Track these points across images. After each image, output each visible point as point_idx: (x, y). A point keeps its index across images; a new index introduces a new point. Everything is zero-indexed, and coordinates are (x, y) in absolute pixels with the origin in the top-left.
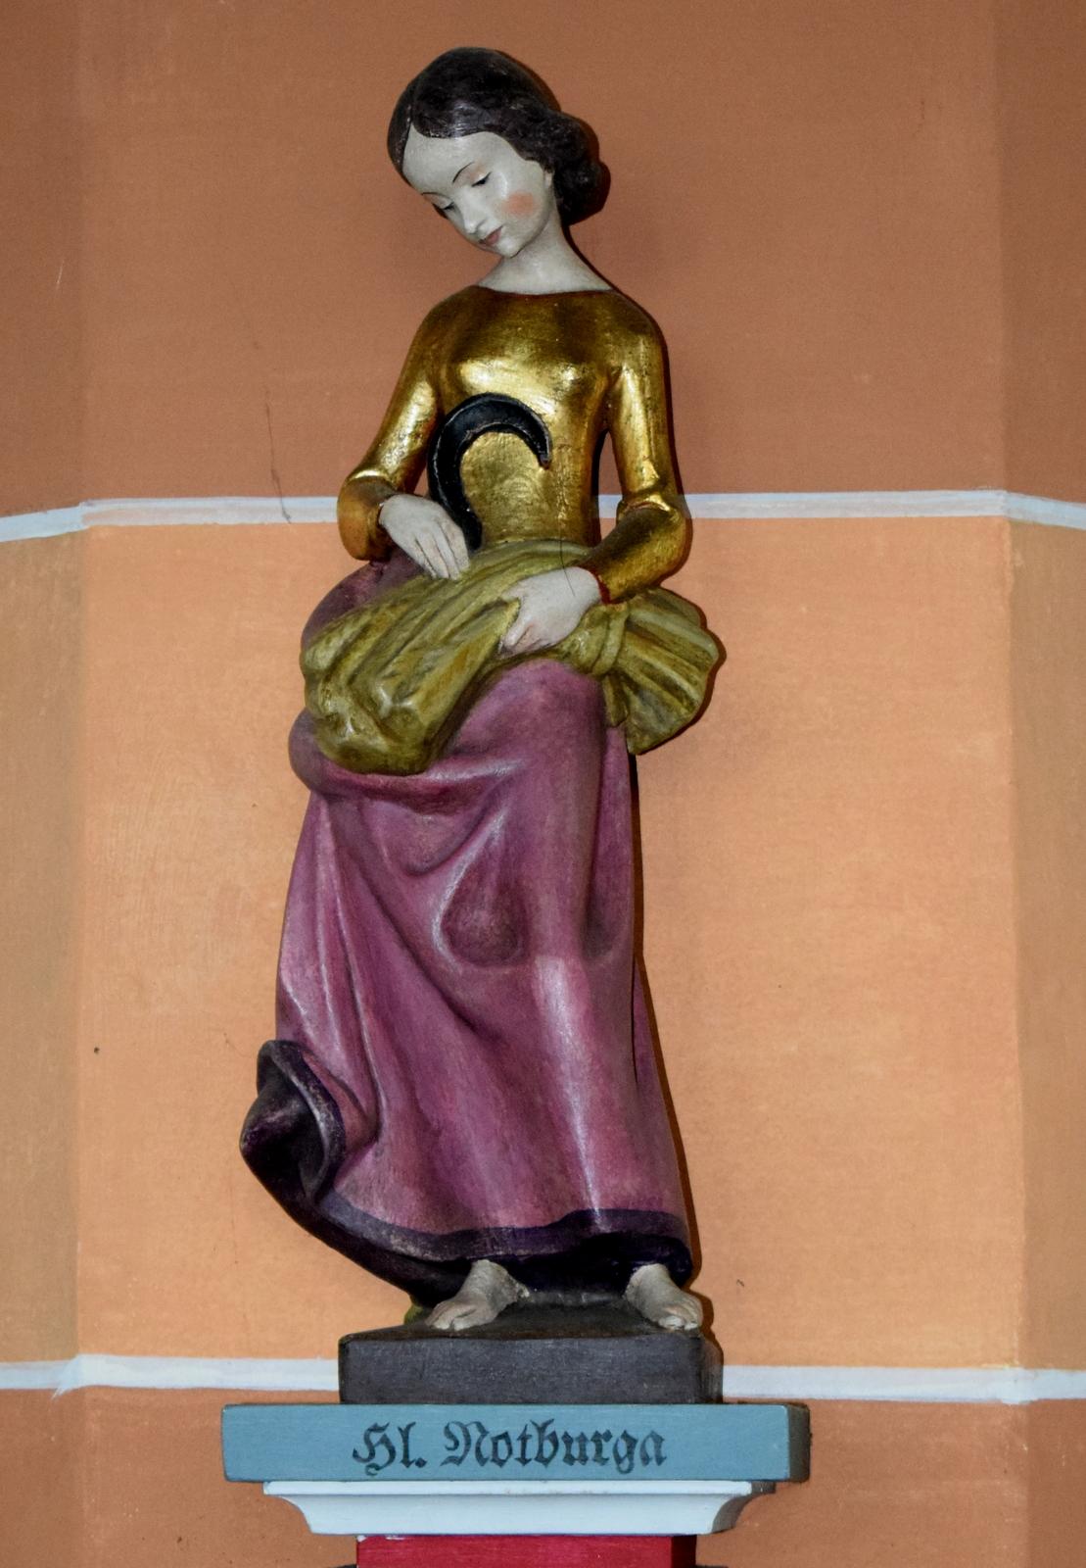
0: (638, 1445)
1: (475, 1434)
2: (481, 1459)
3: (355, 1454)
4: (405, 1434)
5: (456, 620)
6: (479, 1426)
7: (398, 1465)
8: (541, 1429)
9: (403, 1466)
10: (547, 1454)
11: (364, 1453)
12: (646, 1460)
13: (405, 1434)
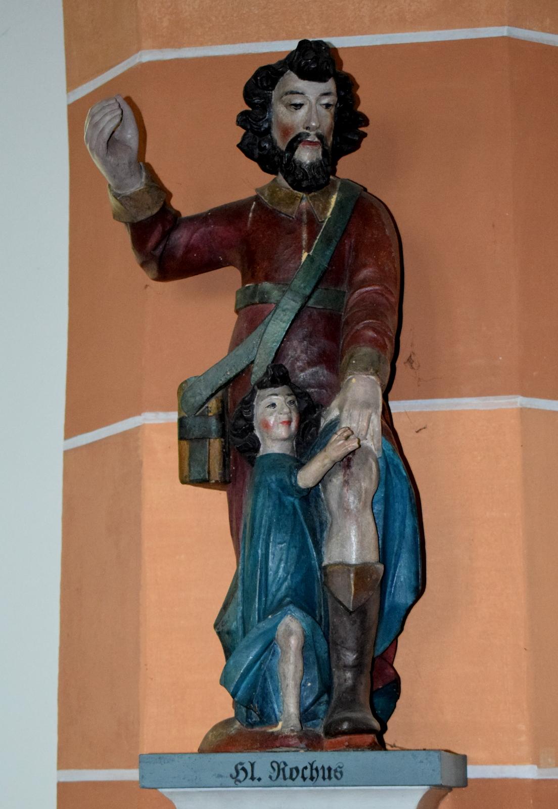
0: (250, 775)
1: (282, 766)
2: (304, 779)
3: (231, 776)
4: (252, 765)
7: (248, 781)
8: (312, 765)
10: (294, 776)
11: (235, 774)
12: (324, 778)
13: (252, 765)
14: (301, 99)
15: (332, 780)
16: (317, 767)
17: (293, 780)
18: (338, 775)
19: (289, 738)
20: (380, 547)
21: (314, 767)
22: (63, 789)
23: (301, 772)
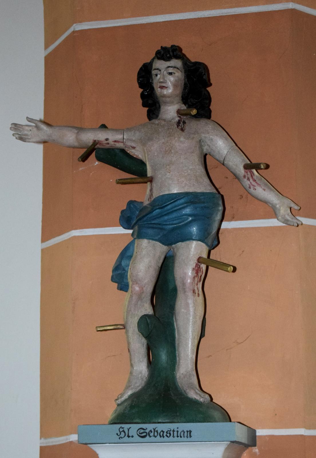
0: (127, 435)
2: (161, 436)
3: (117, 434)
5: (177, 340)
6: (152, 104)
8: (154, 430)
9: (128, 438)
11: (119, 434)
14: (136, 226)
15: (164, 438)
16: (157, 430)
17: (155, 437)
18: (168, 435)
19: (281, 221)
20: (174, 318)
21: (156, 430)
22: (43, 449)
23: (148, 434)
